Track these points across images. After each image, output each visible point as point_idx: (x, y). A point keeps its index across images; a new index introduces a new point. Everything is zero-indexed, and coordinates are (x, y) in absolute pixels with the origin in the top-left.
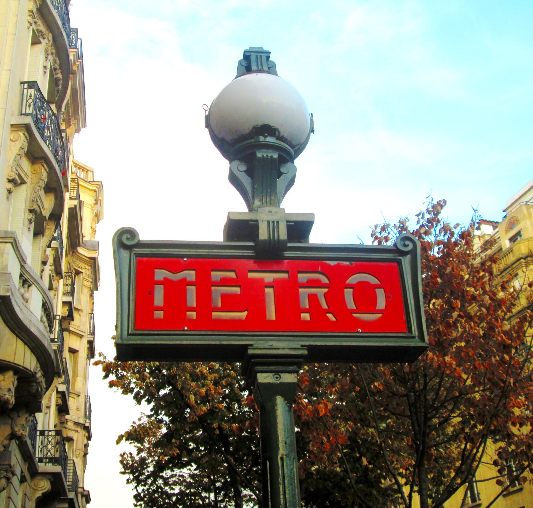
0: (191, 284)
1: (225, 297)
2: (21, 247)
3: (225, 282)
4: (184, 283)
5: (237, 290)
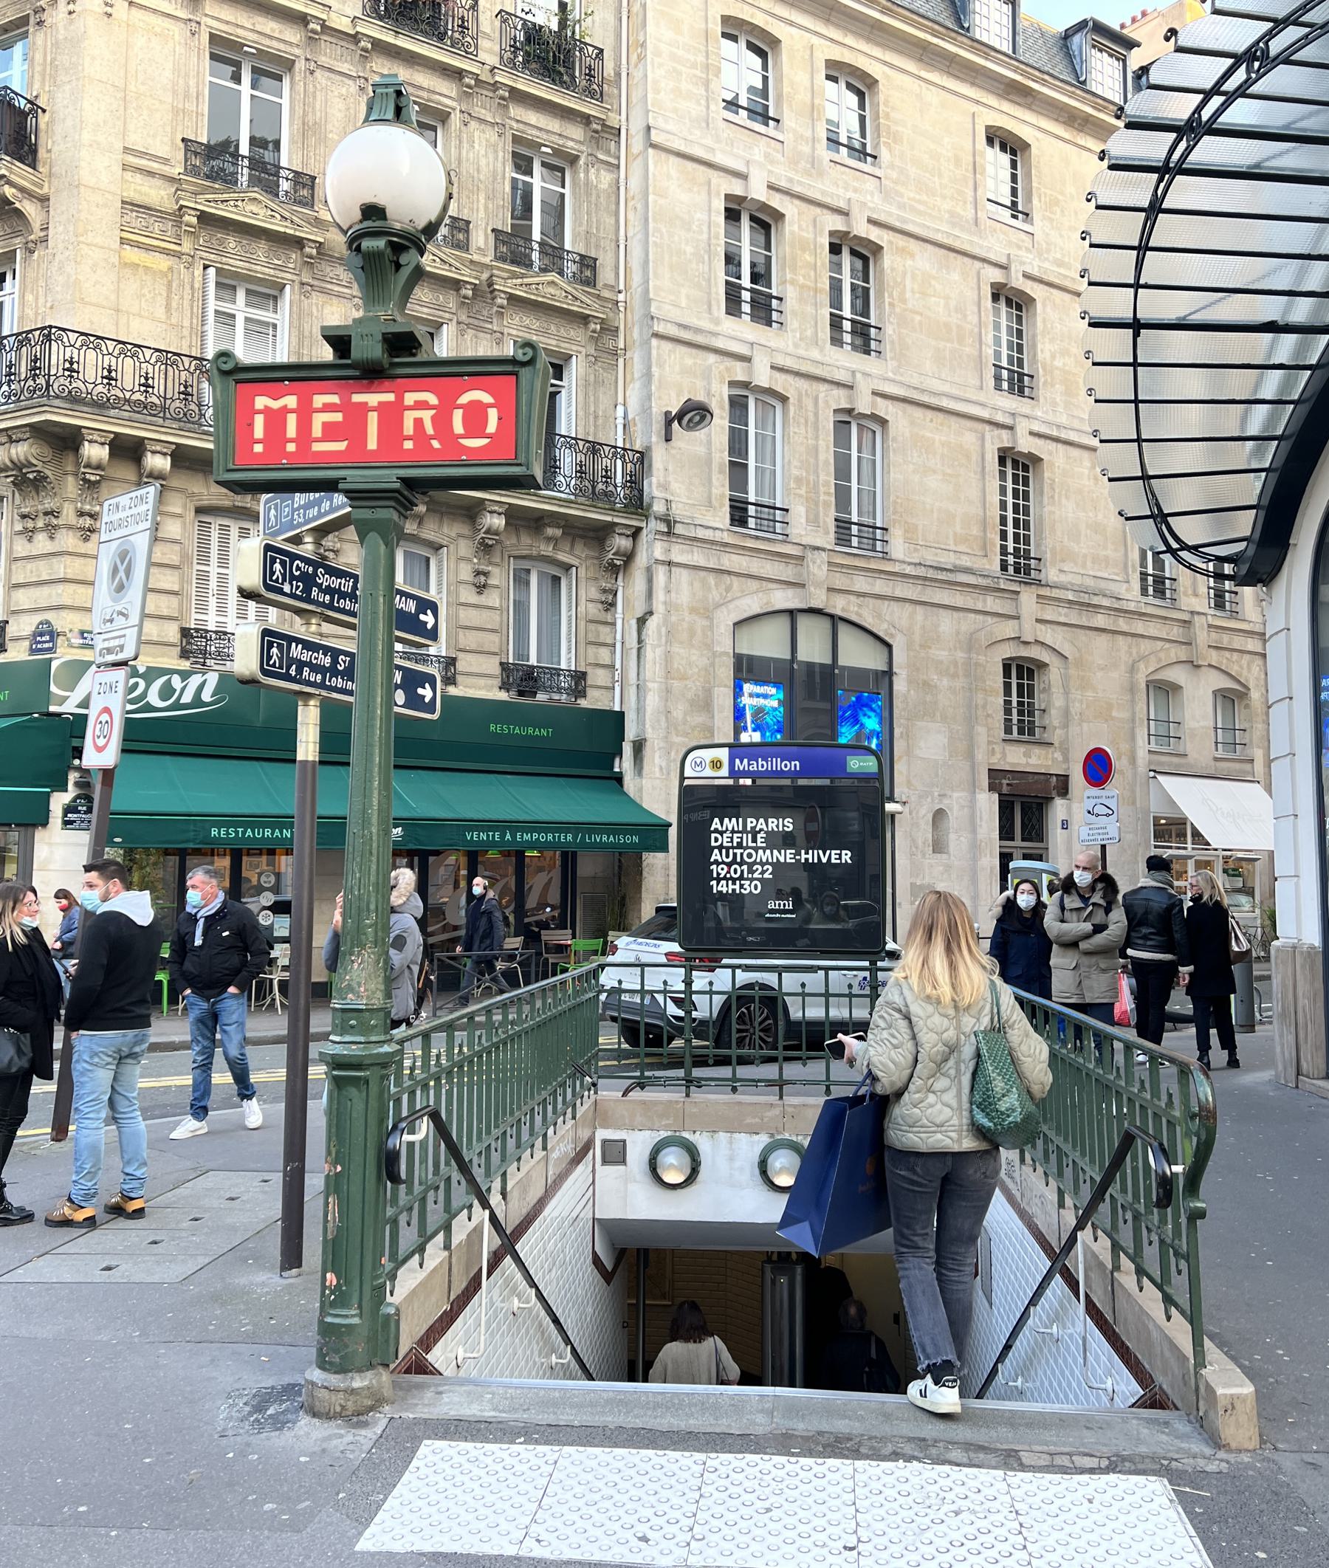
0: (292, 411)
1: (326, 425)
2: (1306, 519)
3: (328, 408)
4: (285, 410)
5: (338, 417)
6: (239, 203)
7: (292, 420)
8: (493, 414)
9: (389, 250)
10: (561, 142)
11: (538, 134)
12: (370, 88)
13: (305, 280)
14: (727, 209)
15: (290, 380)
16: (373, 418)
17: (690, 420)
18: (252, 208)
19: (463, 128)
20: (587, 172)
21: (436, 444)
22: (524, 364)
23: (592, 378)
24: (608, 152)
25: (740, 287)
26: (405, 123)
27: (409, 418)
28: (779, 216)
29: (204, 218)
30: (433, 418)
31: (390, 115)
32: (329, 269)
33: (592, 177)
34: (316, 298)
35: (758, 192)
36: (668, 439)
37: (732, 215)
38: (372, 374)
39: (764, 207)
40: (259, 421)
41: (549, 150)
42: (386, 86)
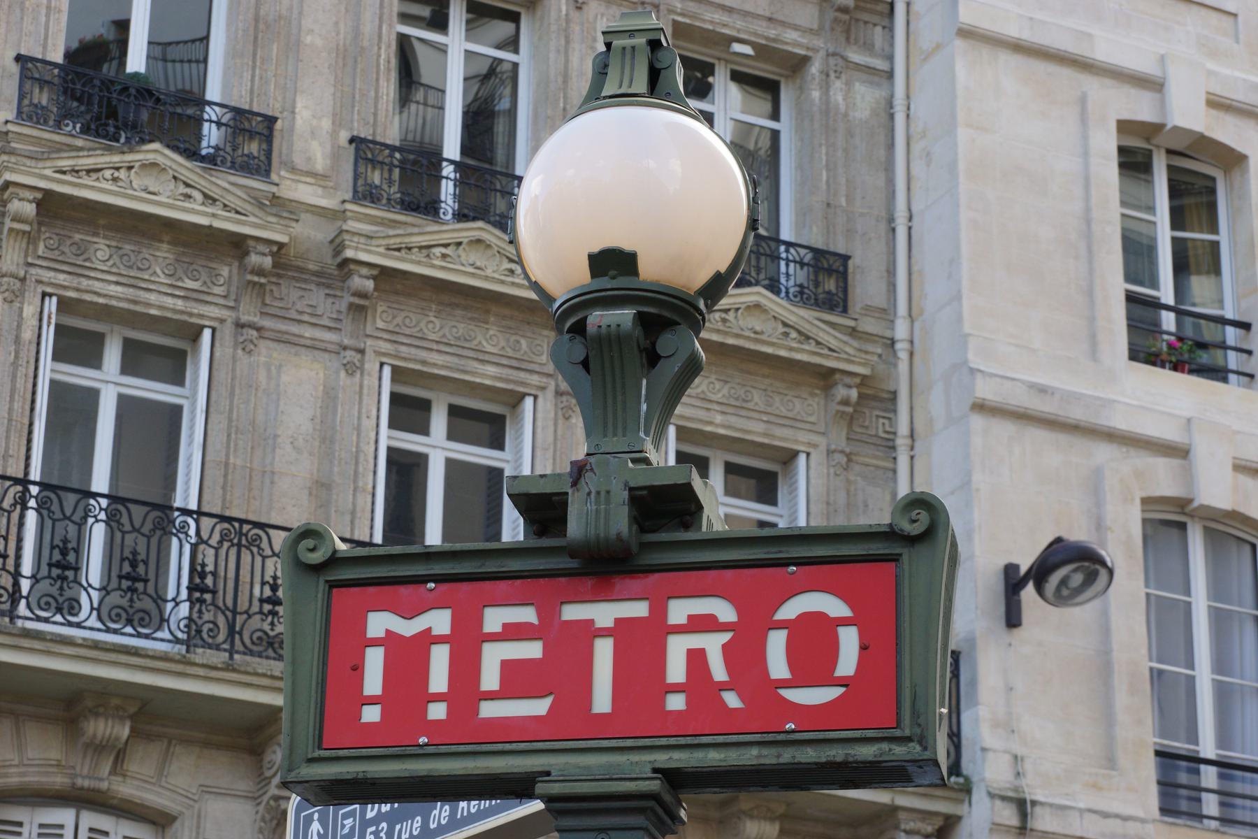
0: (440, 640)
3: (512, 632)
4: (427, 638)
5: (532, 650)
6: (122, 174)
7: (440, 658)
8: (849, 640)
9: (638, 332)
10: (772, 33)
11: (725, 18)
12: (601, 39)
13: (245, 318)
14: (1122, 150)
15: (439, 579)
16: (604, 651)
17: (1064, 582)
18: (146, 180)
19: (575, 15)
20: (826, 88)
21: (732, 700)
22: (912, 540)
23: (841, 498)
24: (868, 47)
25: (1156, 305)
26: (667, 96)
27: (677, 650)
28: (1233, 160)
29: (53, 208)
30: (726, 648)
31: (641, 85)
32: (294, 294)
33: (838, 97)
34: (266, 352)
35: (1187, 112)
36: (1013, 619)
37: (1134, 163)
38: (604, 567)
39: (1203, 145)
40: (374, 660)
41: (747, 50)
42: (631, 33)
